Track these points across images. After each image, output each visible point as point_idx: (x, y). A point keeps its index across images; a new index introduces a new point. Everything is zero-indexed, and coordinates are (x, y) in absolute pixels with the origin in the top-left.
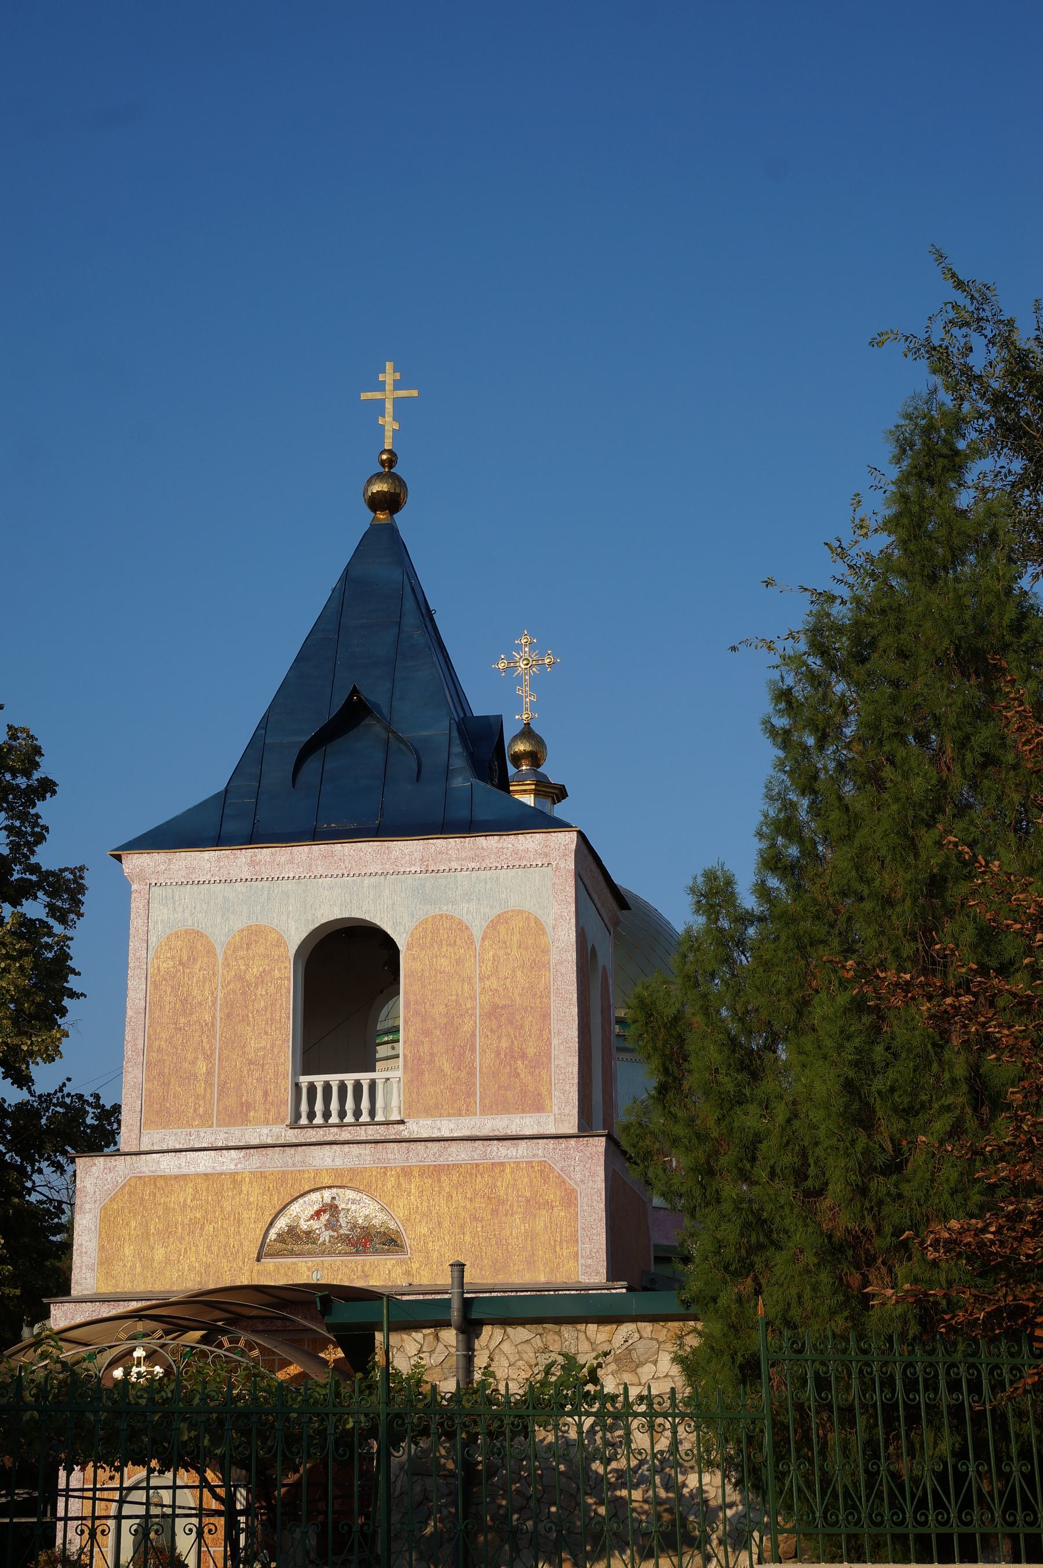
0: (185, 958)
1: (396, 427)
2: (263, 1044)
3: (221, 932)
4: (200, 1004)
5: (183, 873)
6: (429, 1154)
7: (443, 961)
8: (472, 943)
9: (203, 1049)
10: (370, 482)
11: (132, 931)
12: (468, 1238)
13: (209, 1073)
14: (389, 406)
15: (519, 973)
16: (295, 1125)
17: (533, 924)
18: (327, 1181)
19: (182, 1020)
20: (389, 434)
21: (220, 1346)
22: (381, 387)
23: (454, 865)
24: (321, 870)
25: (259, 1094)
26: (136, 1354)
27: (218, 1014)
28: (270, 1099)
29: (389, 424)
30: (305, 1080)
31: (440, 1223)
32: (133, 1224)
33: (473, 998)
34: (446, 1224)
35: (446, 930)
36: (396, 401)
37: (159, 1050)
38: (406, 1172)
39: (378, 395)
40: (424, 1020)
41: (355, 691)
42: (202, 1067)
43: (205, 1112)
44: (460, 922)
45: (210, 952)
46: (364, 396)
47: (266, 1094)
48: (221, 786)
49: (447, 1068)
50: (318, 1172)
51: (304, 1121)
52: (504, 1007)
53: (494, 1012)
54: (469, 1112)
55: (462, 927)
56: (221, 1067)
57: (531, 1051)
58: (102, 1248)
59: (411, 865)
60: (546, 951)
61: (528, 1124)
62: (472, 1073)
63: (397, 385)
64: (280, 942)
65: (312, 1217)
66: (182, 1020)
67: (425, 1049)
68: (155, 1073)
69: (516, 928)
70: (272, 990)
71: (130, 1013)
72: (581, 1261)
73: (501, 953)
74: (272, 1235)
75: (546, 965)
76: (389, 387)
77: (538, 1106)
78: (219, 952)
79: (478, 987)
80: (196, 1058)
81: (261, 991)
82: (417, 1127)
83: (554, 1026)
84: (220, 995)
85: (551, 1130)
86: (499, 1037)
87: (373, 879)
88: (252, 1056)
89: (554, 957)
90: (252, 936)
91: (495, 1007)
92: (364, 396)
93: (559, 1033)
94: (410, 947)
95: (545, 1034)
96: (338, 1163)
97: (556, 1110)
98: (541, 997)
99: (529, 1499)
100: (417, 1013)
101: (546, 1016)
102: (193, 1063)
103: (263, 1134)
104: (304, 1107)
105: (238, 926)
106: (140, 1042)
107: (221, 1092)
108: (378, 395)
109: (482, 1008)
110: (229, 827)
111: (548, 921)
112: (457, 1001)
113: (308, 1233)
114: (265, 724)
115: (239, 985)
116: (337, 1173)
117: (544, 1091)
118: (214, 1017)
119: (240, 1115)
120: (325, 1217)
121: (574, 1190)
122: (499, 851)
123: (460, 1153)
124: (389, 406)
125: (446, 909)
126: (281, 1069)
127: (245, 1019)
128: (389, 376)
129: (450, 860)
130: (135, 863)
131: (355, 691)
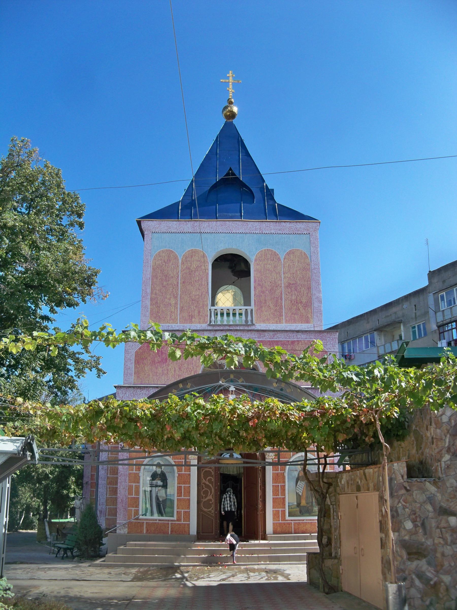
4: (172, 277)
5: (166, 228)
7: (268, 266)
8: (280, 260)
9: (174, 294)
15: (298, 272)
16: (210, 325)
17: (303, 254)
23: (272, 231)
25: (196, 312)
28: (201, 314)
37: (156, 294)
40: (262, 287)
43: (175, 318)
45: (176, 258)
47: (199, 312)
52: (293, 284)
53: (289, 286)
57: (304, 301)
60: (308, 265)
62: (281, 308)
68: (154, 302)
77: (308, 322)
79: (283, 276)
81: (197, 273)
82: (259, 326)
87: (241, 235)
91: (290, 284)
94: (256, 260)
95: (309, 295)
100: (259, 285)
102: (170, 299)
107: (181, 311)
109: (284, 284)
113: (220, 365)
117: (309, 316)
126: (205, 303)
130: (146, 224)
131: (230, 169)
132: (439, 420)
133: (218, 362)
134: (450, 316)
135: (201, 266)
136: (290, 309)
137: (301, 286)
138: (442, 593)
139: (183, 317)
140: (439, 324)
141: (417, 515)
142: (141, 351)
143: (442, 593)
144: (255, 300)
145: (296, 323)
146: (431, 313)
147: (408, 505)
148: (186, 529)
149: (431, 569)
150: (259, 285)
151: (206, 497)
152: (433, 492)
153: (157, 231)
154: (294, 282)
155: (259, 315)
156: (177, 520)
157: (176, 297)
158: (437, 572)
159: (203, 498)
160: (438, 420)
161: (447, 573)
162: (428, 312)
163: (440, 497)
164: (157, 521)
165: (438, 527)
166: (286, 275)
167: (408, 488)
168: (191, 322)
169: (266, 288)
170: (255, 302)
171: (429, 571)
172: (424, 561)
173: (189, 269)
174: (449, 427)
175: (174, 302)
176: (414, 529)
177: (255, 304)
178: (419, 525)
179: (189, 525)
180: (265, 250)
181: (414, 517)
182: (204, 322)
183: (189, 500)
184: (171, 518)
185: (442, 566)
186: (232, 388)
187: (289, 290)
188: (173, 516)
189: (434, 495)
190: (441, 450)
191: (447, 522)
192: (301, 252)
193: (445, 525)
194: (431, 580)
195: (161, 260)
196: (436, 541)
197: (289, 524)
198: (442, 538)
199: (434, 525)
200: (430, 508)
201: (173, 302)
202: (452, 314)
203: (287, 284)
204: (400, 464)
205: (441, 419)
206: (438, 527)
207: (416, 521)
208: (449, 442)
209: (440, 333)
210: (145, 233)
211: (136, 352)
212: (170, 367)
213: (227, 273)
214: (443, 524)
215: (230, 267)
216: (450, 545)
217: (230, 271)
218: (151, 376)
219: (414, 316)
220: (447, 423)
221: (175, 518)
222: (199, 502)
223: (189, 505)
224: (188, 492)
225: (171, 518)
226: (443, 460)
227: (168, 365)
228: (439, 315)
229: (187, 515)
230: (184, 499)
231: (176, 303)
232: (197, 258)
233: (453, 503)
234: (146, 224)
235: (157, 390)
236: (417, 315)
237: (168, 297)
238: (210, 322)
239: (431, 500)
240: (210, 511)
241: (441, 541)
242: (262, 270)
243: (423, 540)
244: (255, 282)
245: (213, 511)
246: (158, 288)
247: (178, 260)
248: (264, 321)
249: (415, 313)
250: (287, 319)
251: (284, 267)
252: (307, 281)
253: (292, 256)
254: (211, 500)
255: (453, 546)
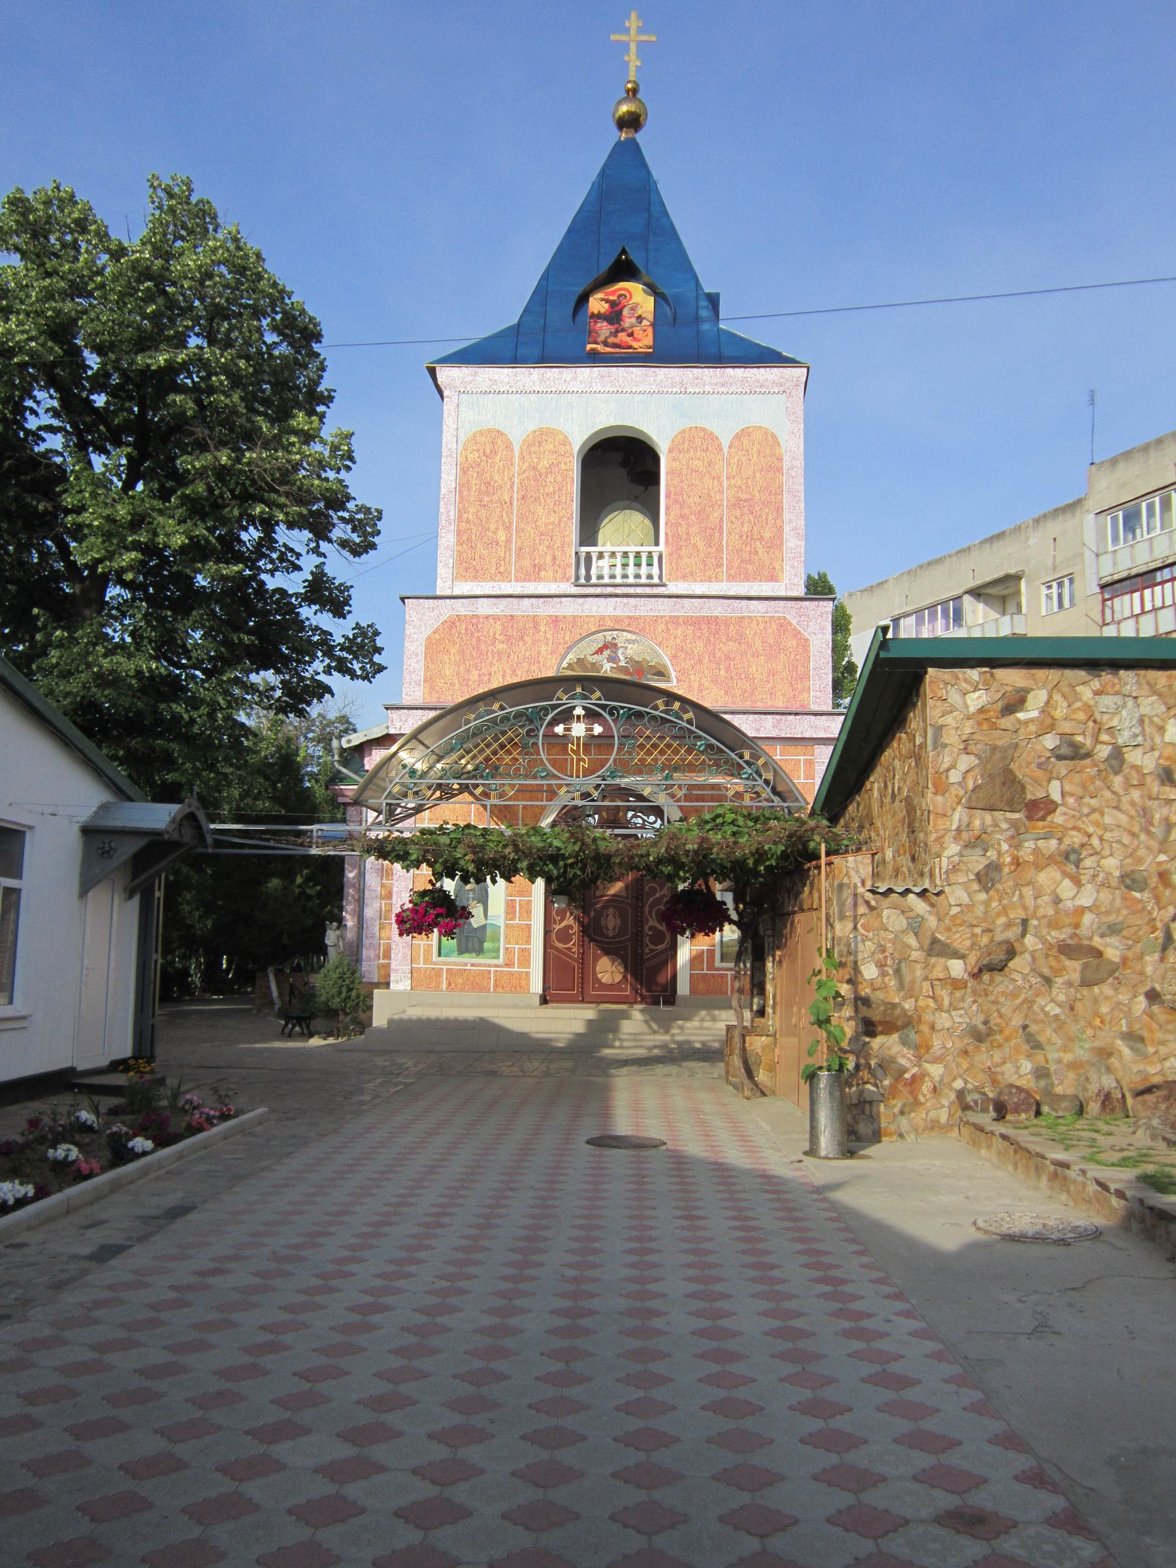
0: (488, 451)
1: (639, 64)
2: (552, 520)
3: (517, 435)
4: (501, 487)
5: (488, 383)
6: (689, 608)
7: (696, 462)
8: (721, 449)
9: (503, 522)
10: (620, 103)
11: (445, 427)
12: (722, 672)
13: (508, 541)
14: (633, 47)
15: (758, 475)
17: (769, 438)
18: (609, 624)
19: (486, 499)
20: (632, 69)
21: (656, 708)
22: (627, 31)
23: (707, 389)
24: (599, 388)
25: (549, 559)
26: (576, 712)
27: (515, 496)
28: (558, 562)
29: (633, 61)
30: (585, 549)
31: (700, 661)
32: (453, 651)
33: (721, 492)
34: (706, 661)
35: (697, 440)
36: (640, 44)
37: (468, 521)
38: (674, 620)
39: (624, 38)
40: (682, 507)
41: (624, 251)
42: (502, 536)
43: (506, 570)
44: (711, 434)
45: (509, 446)
46: (612, 37)
47: (554, 558)
48: (515, 321)
49: (701, 545)
50: (602, 618)
51: (582, 581)
52: (746, 500)
53: (737, 504)
54: (718, 579)
55: (713, 437)
56: (518, 537)
57: (767, 535)
58: (427, 668)
59: (673, 386)
60: (780, 459)
61: (766, 589)
63: (640, 31)
64: (566, 442)
65: (596, 653)
66: (486, 499)
67: (681, 530)
68: (464, 538)
69: (758, 443)
70: (559, 479)
71: (443, 491)
72: (812, 693)
73: (744, 459)
74: (565, 664)
75: (780, 470)
76: (633, 32)
77: (773, 578)
78: (516, 448)
79: (725, 484)
80: (497, 529)
81: (550, 479)
82: (673, 588)
83: (786, 516)
84: (516, 481)
85: (782, 594)
86: (742, 524)
87: (642, 397)
88: (543, 528)
89: (786, 464)
90: (541, 437)
91: (739, 500)
92: (612, 37)
93: (790, 521)
94: (670, 451)
95: (779, 522)
96: (618, 613)
97: (786, 580)
98: (776, 494)
99: (1089, 836)
100: (677, 502)
101: (779, 510)
102: (495, 532)
103: (553, 588)
104: (583, 571)
105: (532, 428)
106: (452, 514)
107: (518, 556)
108: (624, 38)
109: (728, 501)
110: (522, 351)
111: (782, 438)
112: (708, 494)
113: (593, 664)
114: (545, 277)
115: (532, 473)
116: (617, 619)
117: (777, 566)
118: (511, 497)
119: (535, 573)
120: (607, 653)
121: (807, 640)
122: (744, 381)
123: (717, 609)
124: (633, 47)
125: (701, 424)
126: (567, 539)
127: (537, 500)
128: (633, 23)
129: (704, 385)
130: (446, 374)
131: (624, 251)
132: (944, 778)
133: (590, 659)
134: (1129, 565)
135: (559, 463)
136: (739, 551)
137: (763, 503)
138: (925, 1096)
139: (522, 568)
140: (1103, 581)
141: (887, 954)
142: (437, 636)
143: (925, 1096)
144: (667, 534)
145: (748, 580)
146: (1089, 556)
147: (871, 935)
148: (523, 982)
149: (910, 1053)
150: (677, 502)
151: (561, 921)
152: (921, 913)
153: (469, 389)
154: (749, 497)
155: (674, 565)
156: (507, 965)
157: (508, 528)
158: (919, 1058)
159: (555, 923)
160: (940, 778)
161: (936, 1060)
162: (1082, 555)
163: (935, 923)
164: (469, 967)
165: (926, 978)
166: (733, 482)
167: (873, 903)
168: (538, 579)
169: (689, 507)
170: (667, 538)
171: (904, 1056)
172: (895, 1036)
173: (535, 468)
174: (962, 792)
175: (503, 538)
176: (880, 979)
177: (667, 542)
178: (891, 972)
179: (528, 974)
180: (690, 429)
181: (881, 956)
182: (564, 579)
183: (529, 927)
184: (494, 961)
185: (928, 1048)
186: (579, 711)
187: (738, 513)
188: (498, 957)
189: (923, 918)
190: (943, 836)
191: (947, 968)
192: (766, 433)
193: (941, 976)
194: (906, 1070)
195: (478, 450)
196: (921, 1003)
197: (722, 976)
198: (933, 998)
199: (919, 973)
200: (912, 941)
201: (502, 536)
202: (1133, 559)
203: (733, 500)
204: (859, 858)
205: (947, 777)
206: (926, 978)
207: (885, 965)
208: (960, 820)
209: (1104, 601)
210: (445, 394)
211: (429, 638)
212: (494, 669)
213: (618, 475)
214: (938, 973)
215: (624, 464)
216: (948, 1012)
217: (623, 472)
218: (457, 686)
219: (1050, 562)
220: (959, 783)
221: (501, 961)
222: (547, 933)
223: (529, 936)
224: (527, 912)
225: (494, 961)
226: (946, 853)
227: (491, 664)
228: (1106, 560)
229: (525, 956)
230: (519, 926)
231: (508, 541)
232: (551, 446)
233: (958, 935)
234: (446, 374)
235: (438, 712)
236: (1058, 560)
237: (492, 527)
238: (577, 578)
239: (916, 926)
240: (569, 949)
241: (931, 1002)
242: (684, 472)
243: (897, 1000)
244: (668, 496)
245: (575, 949)
246: (471, 510)
247: (512, 450)
248: (684, 578)
249: (1054, 556)
250: (732, 572)
251: (729, 464)
252: (776, 494)
253: (745, 442)
254: (571, 927)
255: (954, 1013)
